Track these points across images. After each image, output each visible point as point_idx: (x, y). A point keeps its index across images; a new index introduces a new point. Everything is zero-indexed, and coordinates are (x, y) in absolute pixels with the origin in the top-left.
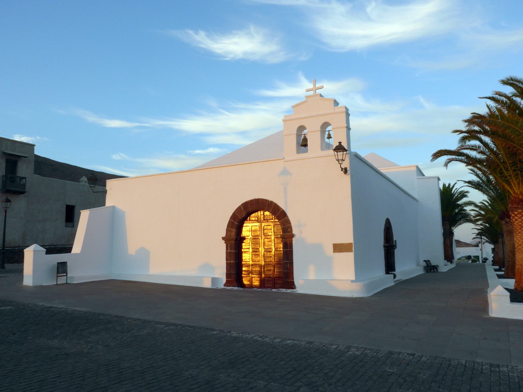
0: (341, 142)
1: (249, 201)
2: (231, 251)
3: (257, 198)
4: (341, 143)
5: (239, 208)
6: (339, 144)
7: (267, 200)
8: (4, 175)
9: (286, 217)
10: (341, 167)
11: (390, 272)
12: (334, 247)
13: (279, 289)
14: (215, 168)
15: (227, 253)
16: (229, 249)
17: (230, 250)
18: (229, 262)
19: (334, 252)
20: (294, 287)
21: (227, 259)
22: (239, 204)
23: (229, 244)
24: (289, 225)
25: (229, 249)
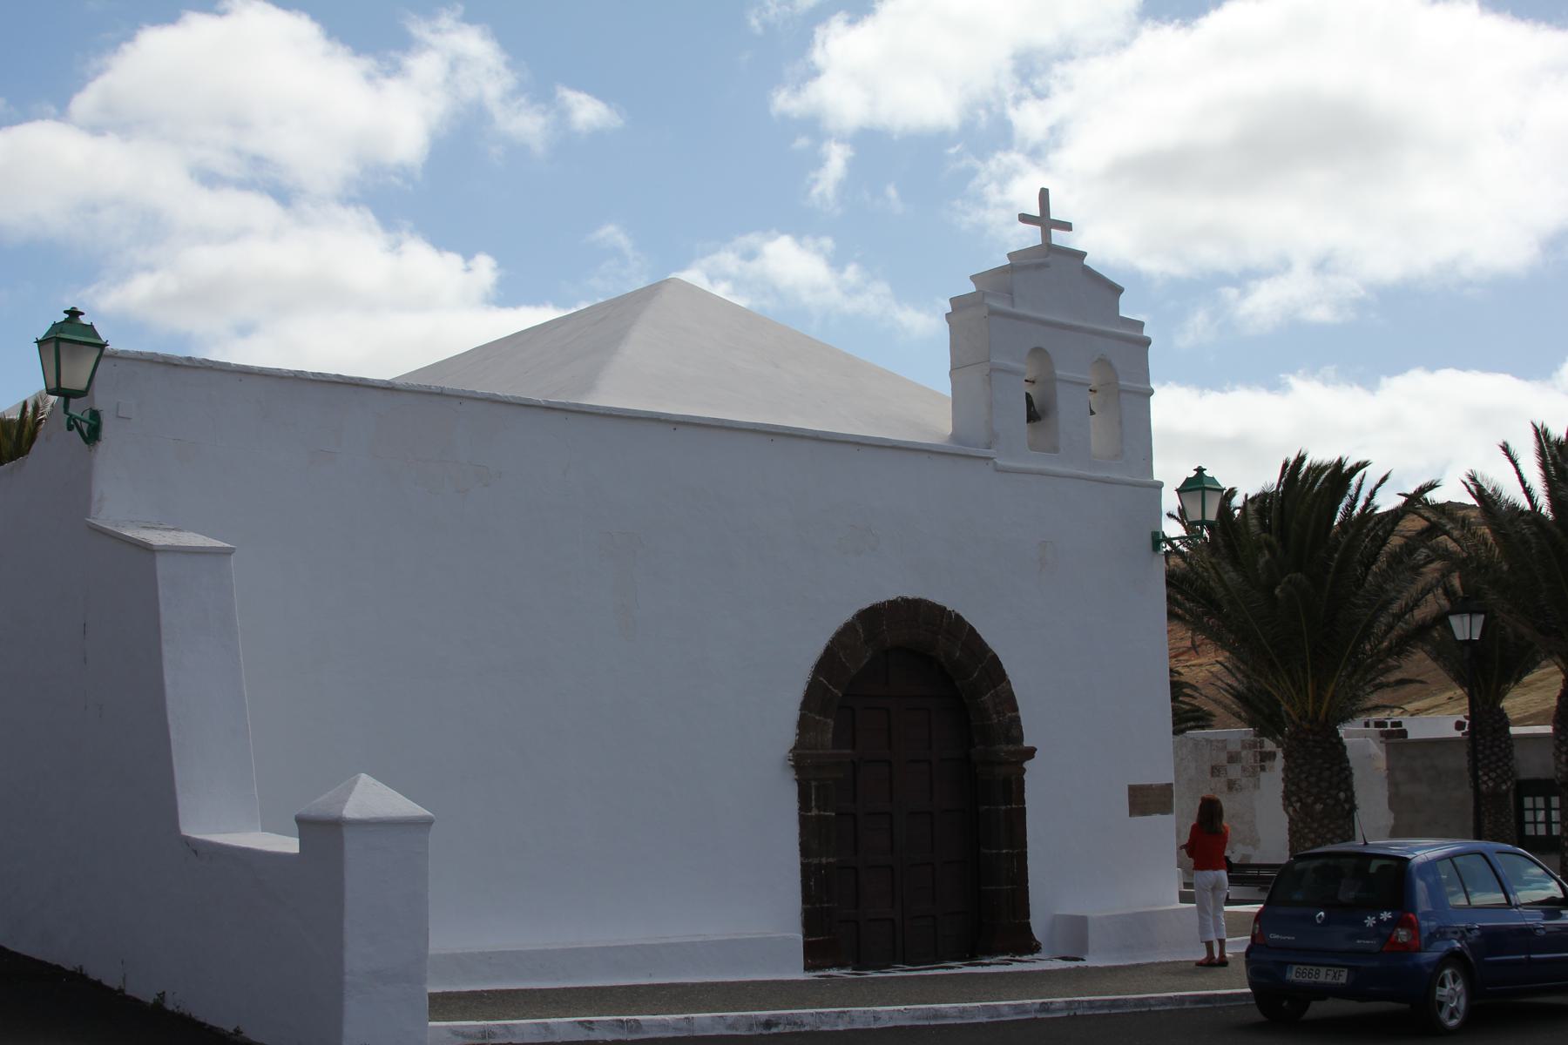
0: (1204, 467)
1: (884, 604)
2: (822, 813)
3: (910, 595)
4: (1204, 472)
5: (847, 630)
6: (1196, 472)
7: (943, 609)
8: (951, 311)
9: (1004, 684)
10: (66, 411)
11: (1394, 863)
12: (1130, 796)
13: (830, 967)
14: (1041, 473)
15: (804, 822)
16: (813, 803)
17: (818, 808)
18: (816, 861)
19: (1130, 815)
20: (1034, 944)
21: (805, 850)
22: (847, 615)
23: (813, 783)
24: (1014, 714)
25: (813, 803)
